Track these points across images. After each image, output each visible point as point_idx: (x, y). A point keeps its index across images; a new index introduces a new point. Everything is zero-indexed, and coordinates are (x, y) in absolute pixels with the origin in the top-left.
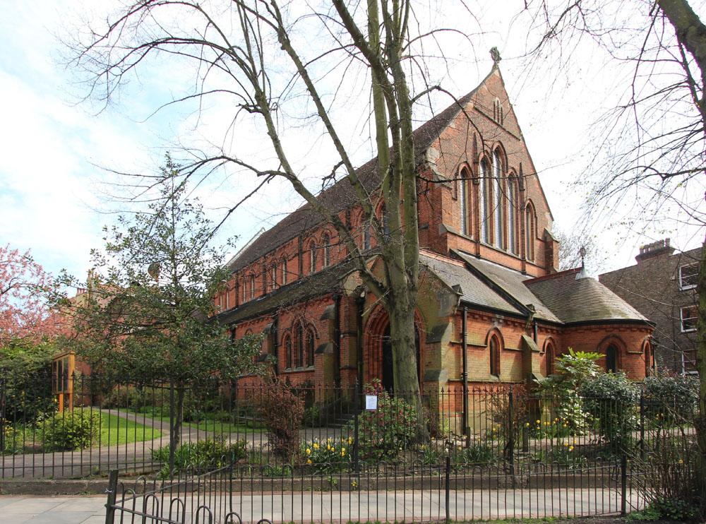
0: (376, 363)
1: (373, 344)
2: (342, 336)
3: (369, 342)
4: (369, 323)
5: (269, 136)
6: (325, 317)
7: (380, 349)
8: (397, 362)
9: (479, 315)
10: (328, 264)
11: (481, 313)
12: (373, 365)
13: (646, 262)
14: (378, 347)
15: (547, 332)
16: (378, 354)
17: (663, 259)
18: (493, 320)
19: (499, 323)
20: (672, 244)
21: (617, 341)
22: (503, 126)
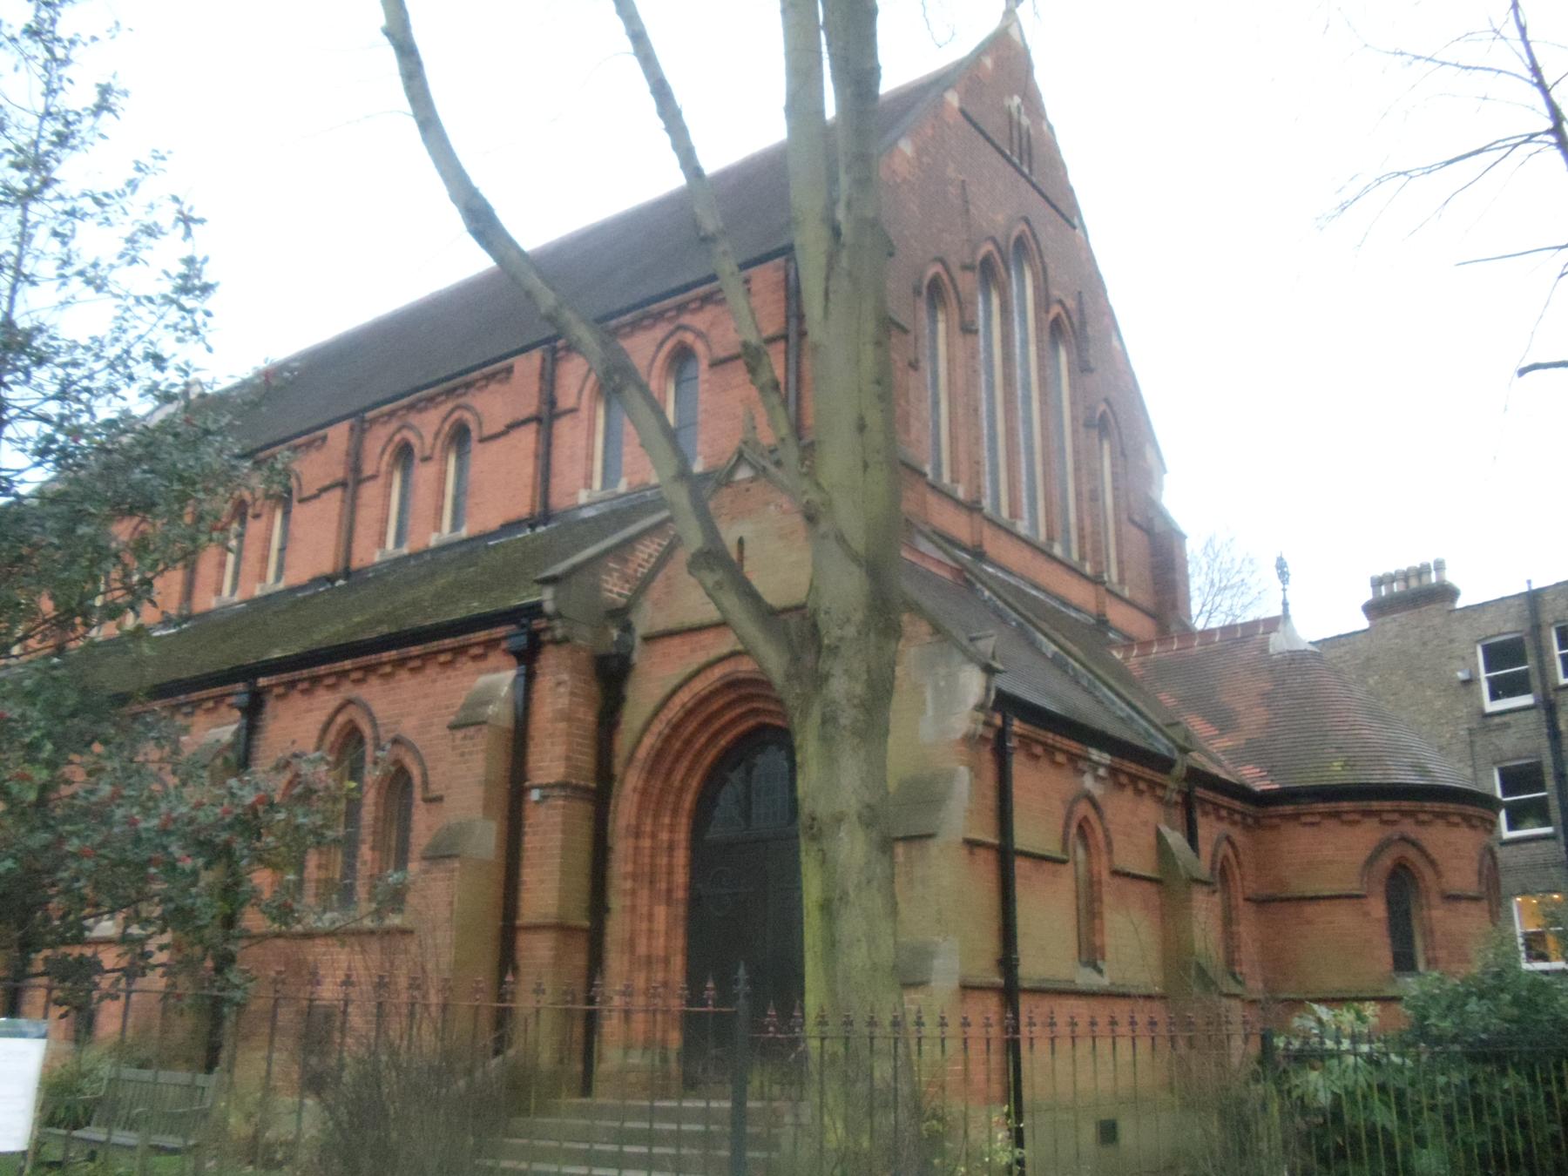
0: (661, 911)
1: (654, 836)
2: (535, 795)
3: (638, 826)
4: (642, 753)
5: (385, 40)
6: (466, 722)
7: (681, 857)
8: (826, 907)
9: (1044, 744)
10: (455, 526)
11: (1050, 737)
12: (651, 917)
13: (1393, 623)
14: (671, 847)
15: (1220, 818)
16: (670, 873)
17: (1432, 614)
18: (1081, 764)
19: (1097, 778)
20: (1452, 577)
21: (1412, 854)
22: (1034, 179)
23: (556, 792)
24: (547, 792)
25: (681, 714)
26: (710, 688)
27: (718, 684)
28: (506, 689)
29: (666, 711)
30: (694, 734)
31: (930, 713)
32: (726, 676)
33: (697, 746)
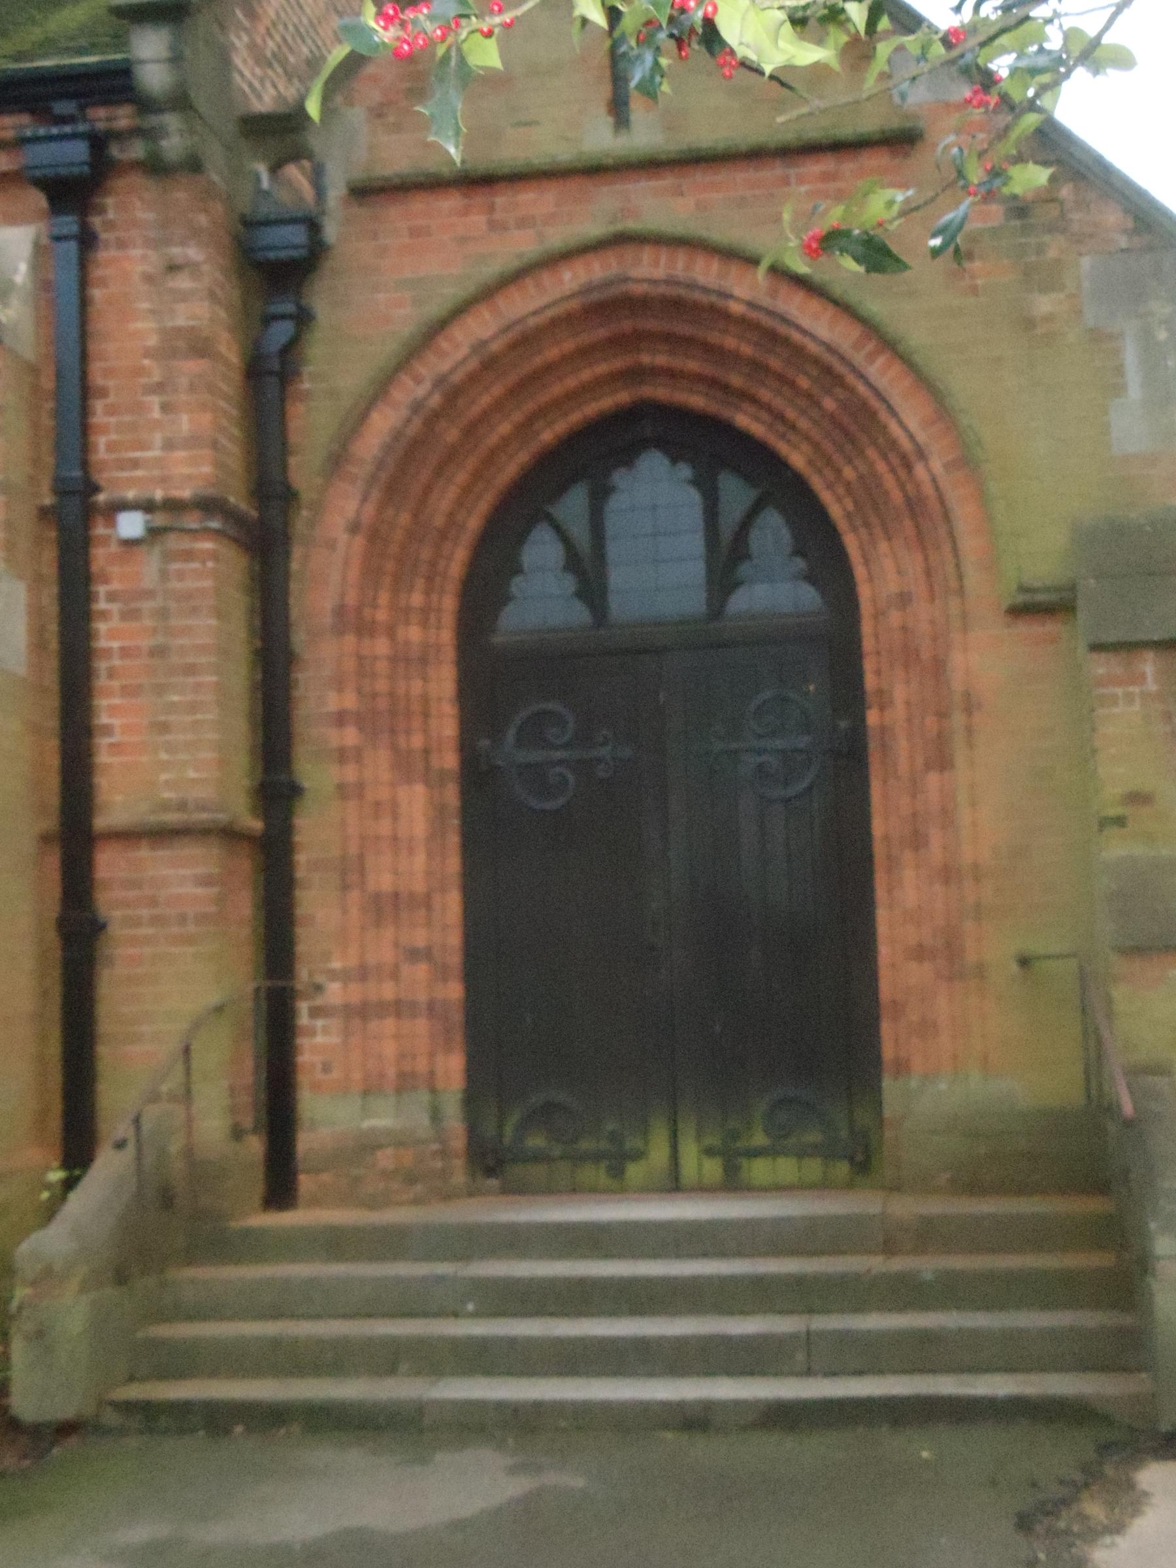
23: (192, 521)
24: (160, 520)
25: (473, 364)
26: (550, 313)
27: (574, 304)
28: (23, 267)
29: (431, 357)
30: (485, 417)
31: (1135, 391)
32: (588, 289)
33: (493, 440)
